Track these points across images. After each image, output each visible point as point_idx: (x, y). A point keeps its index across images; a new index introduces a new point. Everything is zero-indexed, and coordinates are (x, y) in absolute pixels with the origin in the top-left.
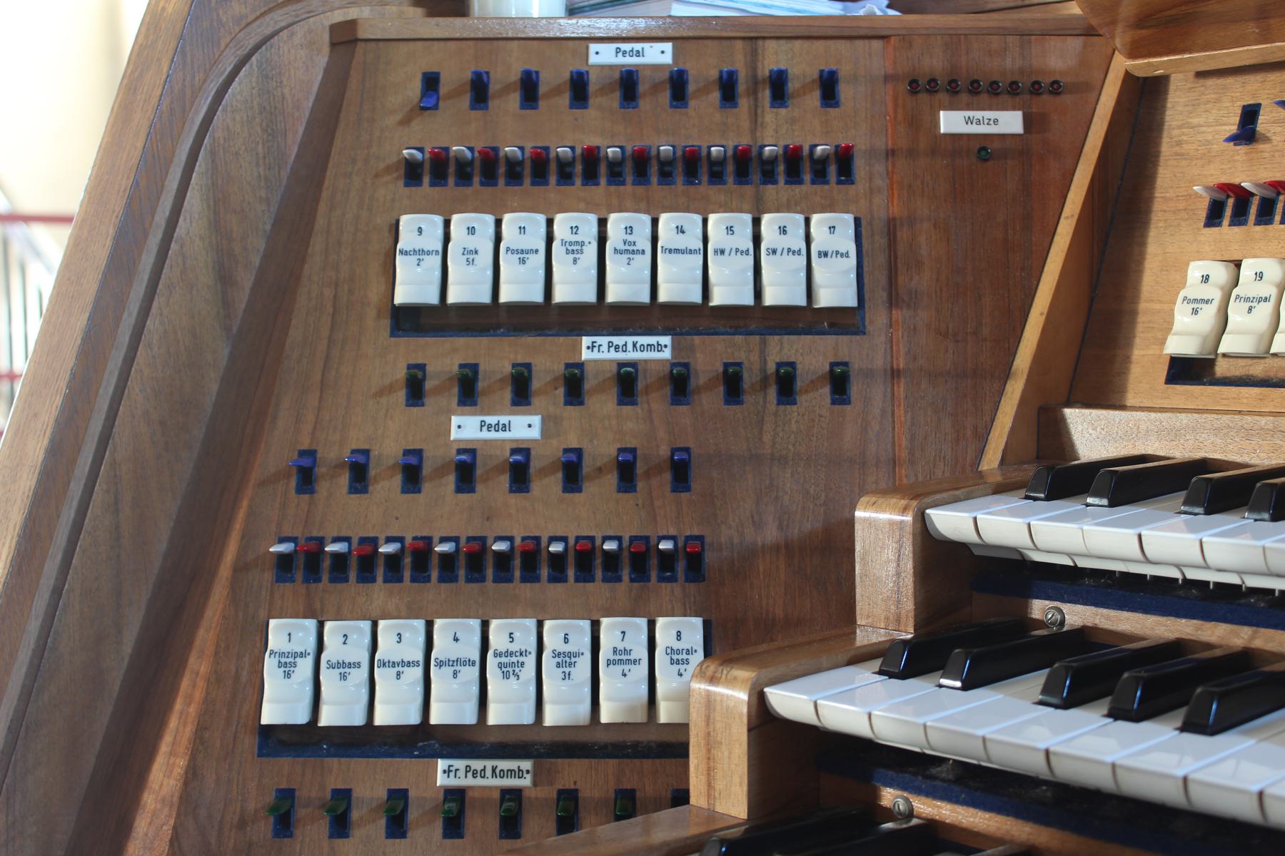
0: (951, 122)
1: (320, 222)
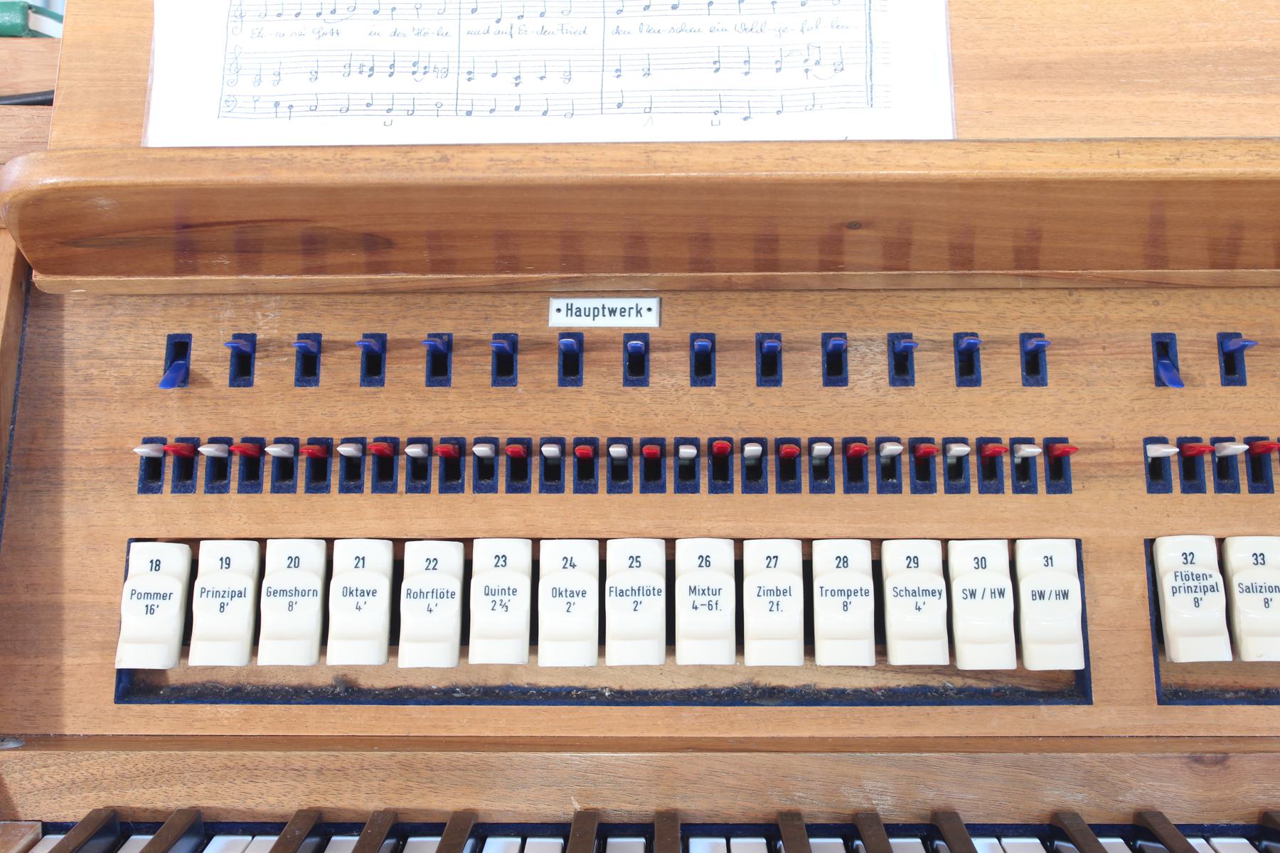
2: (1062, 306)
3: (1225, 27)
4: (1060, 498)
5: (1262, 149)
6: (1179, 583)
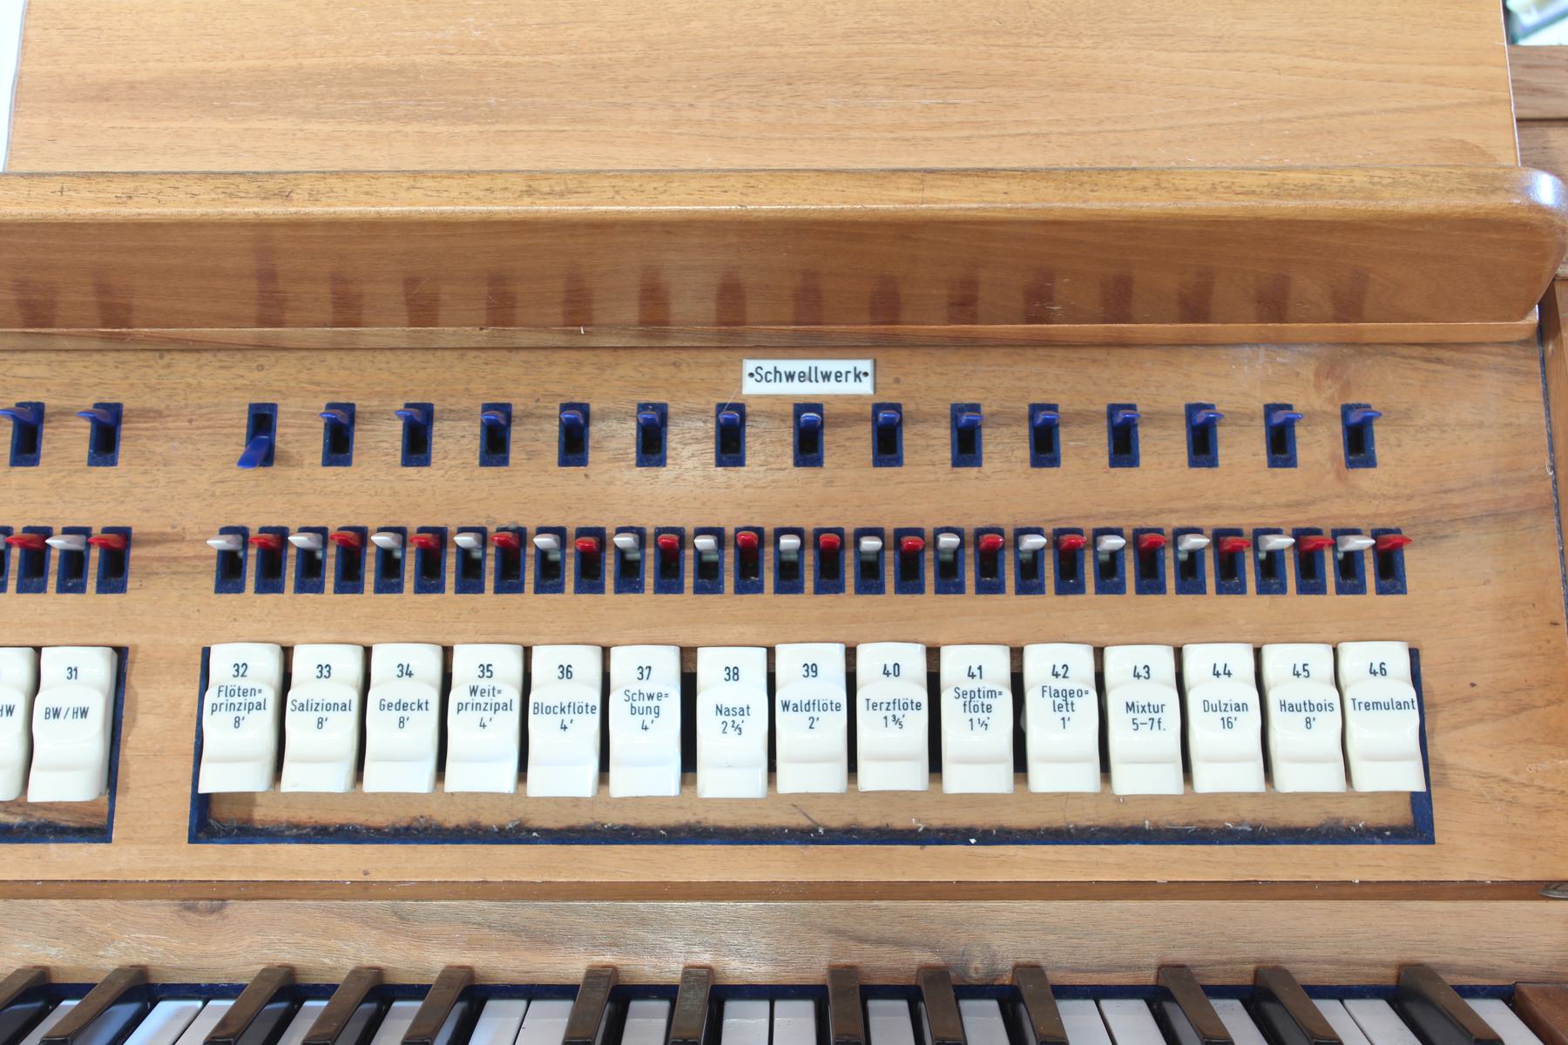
2: (149, 371)
3: (349, 40)
5: (230, 186)
6: (222, 699)
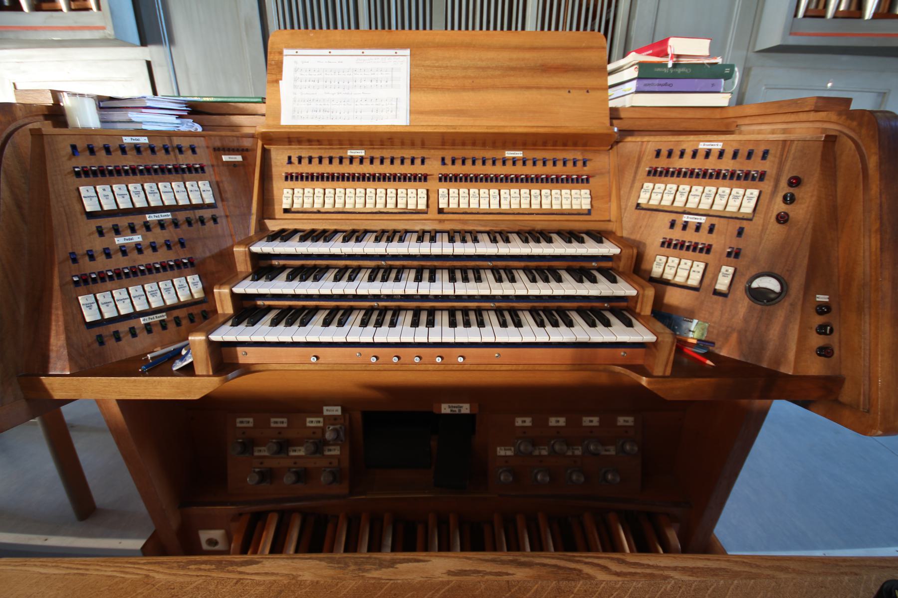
0: (225, 158)
1: (51, 190)
4: (426, 183)
